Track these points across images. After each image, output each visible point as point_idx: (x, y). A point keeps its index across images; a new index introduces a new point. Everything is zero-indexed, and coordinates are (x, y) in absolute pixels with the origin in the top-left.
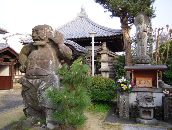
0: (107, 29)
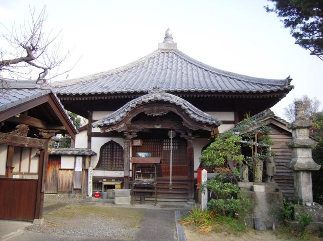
0: (242, 78)
